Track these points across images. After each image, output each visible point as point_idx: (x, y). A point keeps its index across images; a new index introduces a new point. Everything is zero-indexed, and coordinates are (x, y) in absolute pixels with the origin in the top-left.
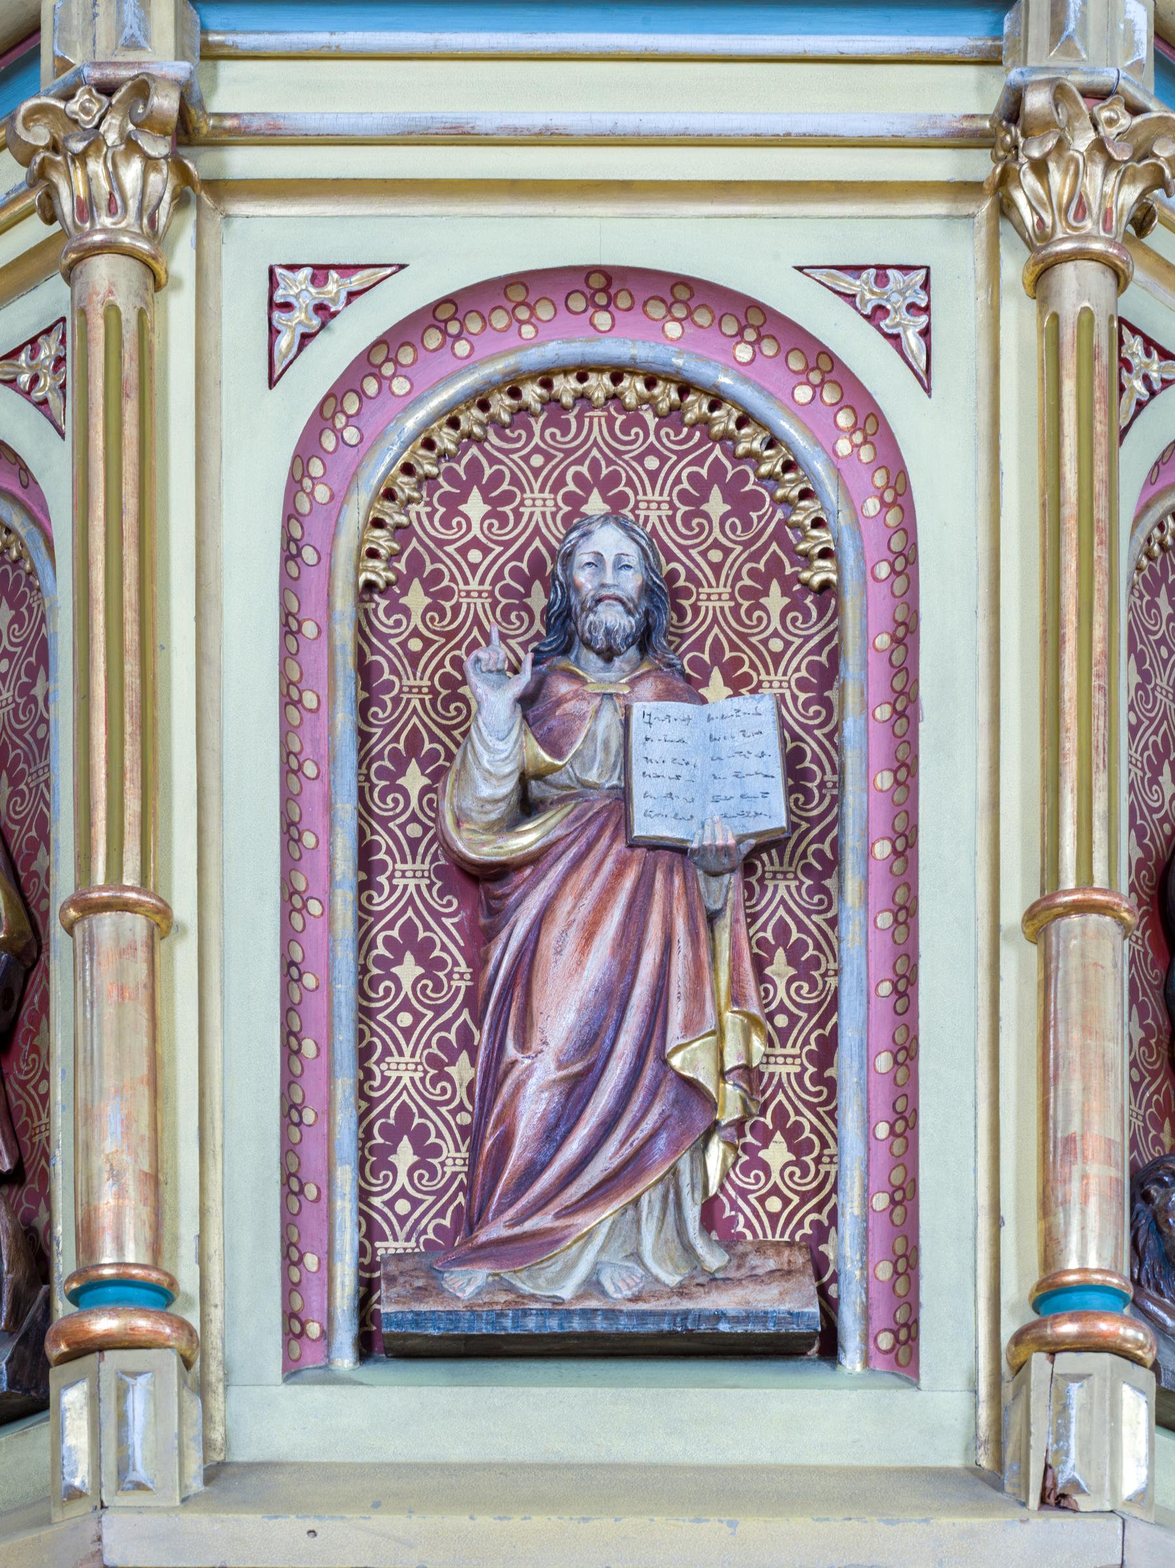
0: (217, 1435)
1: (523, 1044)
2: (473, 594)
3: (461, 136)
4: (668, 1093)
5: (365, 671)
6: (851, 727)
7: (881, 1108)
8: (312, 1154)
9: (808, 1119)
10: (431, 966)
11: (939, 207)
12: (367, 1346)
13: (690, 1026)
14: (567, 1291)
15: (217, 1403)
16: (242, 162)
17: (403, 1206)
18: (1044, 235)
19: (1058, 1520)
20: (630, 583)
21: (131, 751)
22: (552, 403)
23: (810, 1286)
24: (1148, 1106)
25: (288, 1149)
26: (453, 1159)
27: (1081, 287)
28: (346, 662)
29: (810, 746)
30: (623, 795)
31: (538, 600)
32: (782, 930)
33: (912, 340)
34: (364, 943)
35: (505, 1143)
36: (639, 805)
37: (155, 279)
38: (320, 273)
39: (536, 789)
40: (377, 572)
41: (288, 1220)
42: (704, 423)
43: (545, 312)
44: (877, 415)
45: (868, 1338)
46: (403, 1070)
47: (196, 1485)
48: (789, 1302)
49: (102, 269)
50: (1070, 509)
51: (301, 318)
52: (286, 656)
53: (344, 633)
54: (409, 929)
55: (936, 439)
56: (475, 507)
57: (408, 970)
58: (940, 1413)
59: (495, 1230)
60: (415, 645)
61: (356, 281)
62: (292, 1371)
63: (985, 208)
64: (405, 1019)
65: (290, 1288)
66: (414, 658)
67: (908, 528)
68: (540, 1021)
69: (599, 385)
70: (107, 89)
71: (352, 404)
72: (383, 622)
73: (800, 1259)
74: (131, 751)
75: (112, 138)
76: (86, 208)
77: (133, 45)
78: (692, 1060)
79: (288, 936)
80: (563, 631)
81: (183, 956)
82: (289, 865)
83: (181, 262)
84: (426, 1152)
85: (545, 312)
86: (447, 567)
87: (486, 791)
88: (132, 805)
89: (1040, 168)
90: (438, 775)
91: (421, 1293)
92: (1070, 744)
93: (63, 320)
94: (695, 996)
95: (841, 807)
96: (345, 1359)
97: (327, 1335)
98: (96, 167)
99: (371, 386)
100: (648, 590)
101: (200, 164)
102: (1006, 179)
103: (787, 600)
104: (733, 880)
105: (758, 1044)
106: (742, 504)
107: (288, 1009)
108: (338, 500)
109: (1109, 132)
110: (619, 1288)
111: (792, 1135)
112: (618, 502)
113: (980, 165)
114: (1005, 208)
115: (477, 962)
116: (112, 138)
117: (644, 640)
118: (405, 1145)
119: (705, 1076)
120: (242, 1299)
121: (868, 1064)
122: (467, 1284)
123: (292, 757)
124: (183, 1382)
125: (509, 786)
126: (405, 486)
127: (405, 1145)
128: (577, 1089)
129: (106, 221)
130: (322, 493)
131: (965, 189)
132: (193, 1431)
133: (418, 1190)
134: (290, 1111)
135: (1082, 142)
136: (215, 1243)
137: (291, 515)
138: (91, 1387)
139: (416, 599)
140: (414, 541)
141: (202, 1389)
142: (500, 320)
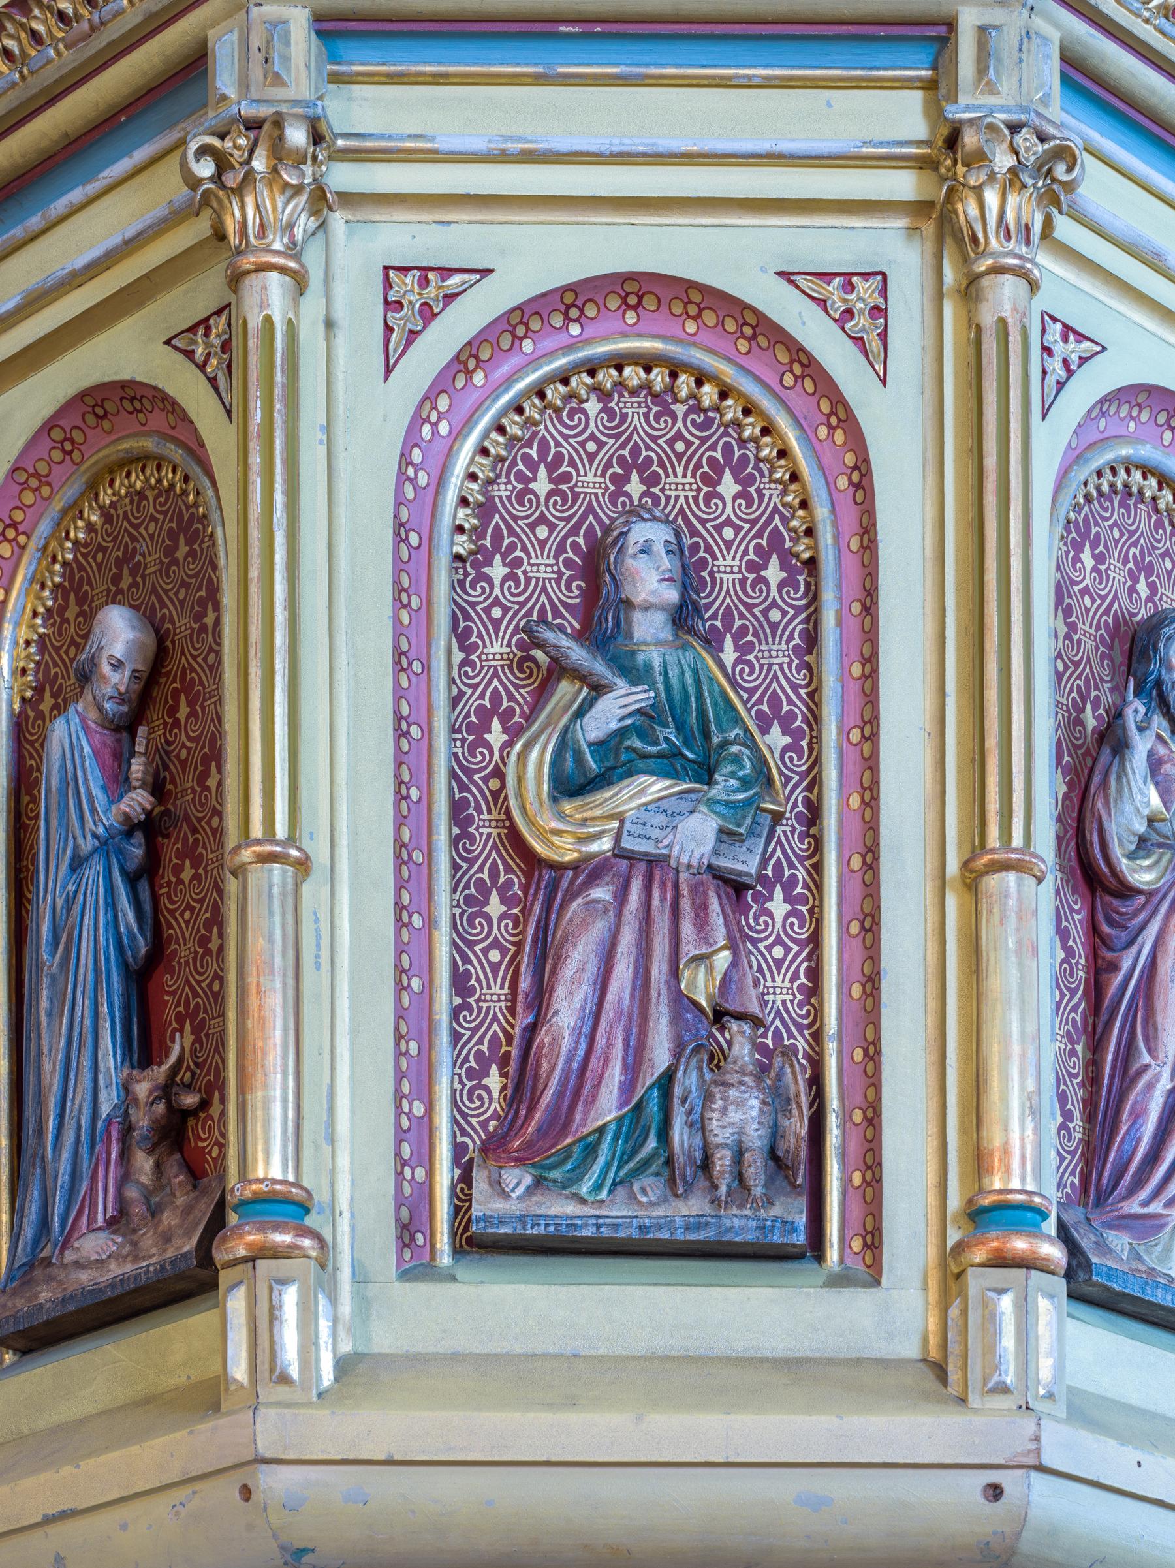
24: (1098, 628)
38: (878, 311)
58: (896, 1315)
60: (497, 613)
66: (497, 623)
93: (229, 305)
95: (821, 766)
103: (784, 575)
123: (403, 786)
138: (248, 1289)
140: (497, 516)
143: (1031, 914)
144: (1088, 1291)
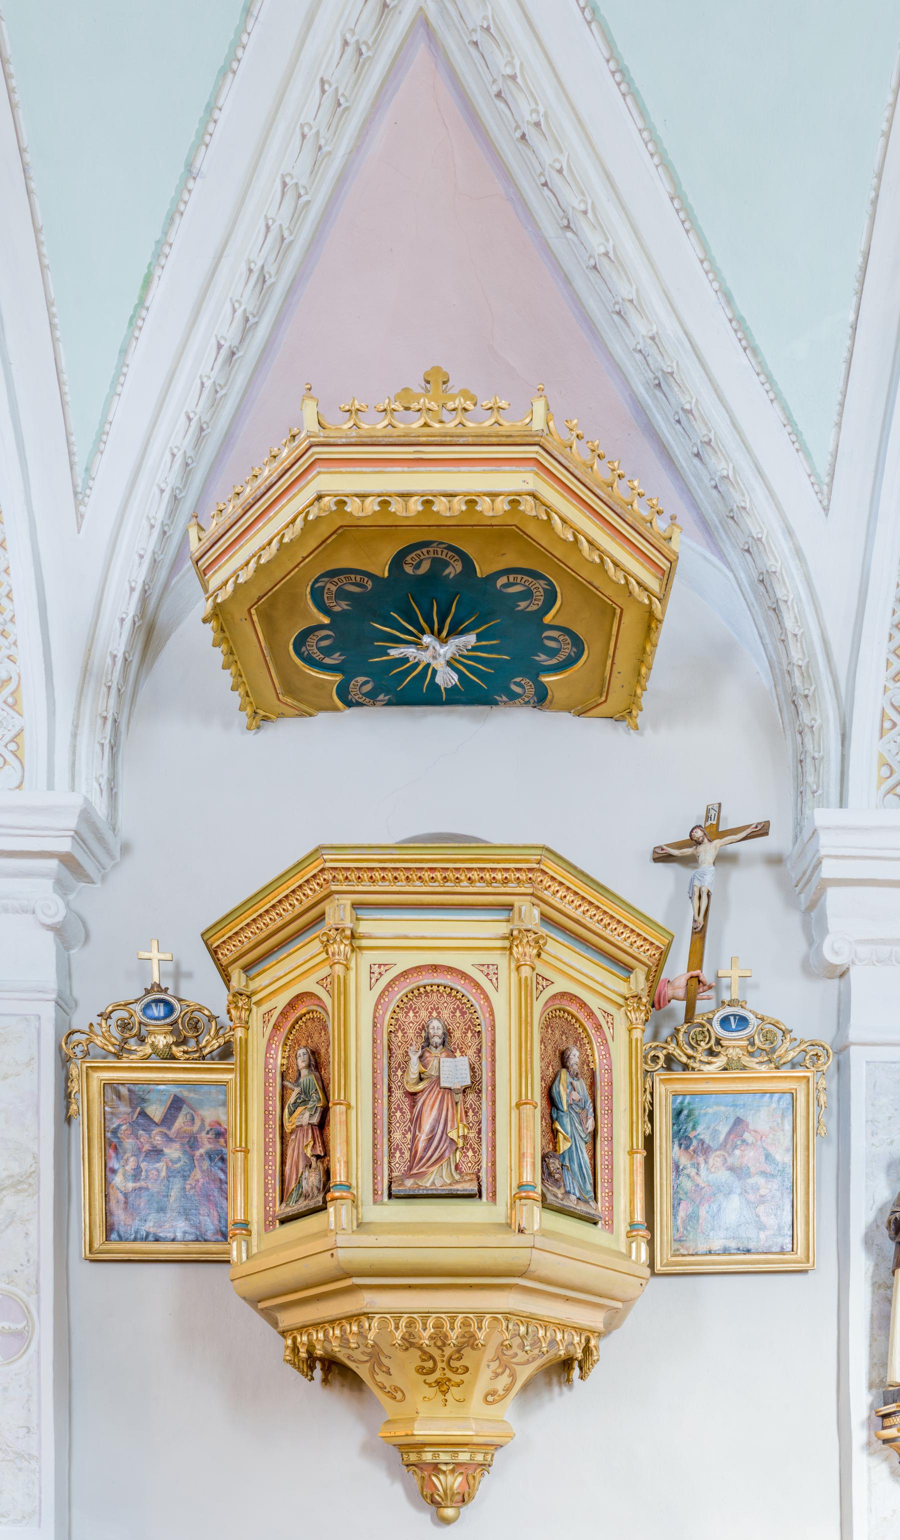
0: (360, 1216)
1: (419, 1131)
2: (411, 1033)
3: (406, 937)
4: (448, 1141)
5: (390, 1049)
6: (484, 1063)
7: (490, 1145)
8: (379, 1154)
9: (476, 1146)
10: (403, 1113)
11: (499, 952)
12: (390, 1196)
13: (452, 1127)
14: (428, 1185)
15: (360, 1209)
16: (364, 943)
17: (397, 1165)
18: (518, 960)
19: (521, 1236)
20: (440, 1032)
21: (342, 1070)
22: (426, 992)
23: (476, 1183)
25: (374, 1154)
26: (407, 1155)
27: (526, 971)
28: (386, 1049)
29: (476, 1066)
30: (439, 1077)
31: (423, 1034)
32: (471, 1105)
33: (494, 980)
34: (389, 1108)
35: (416, 1152)
36: (442, 1080)
37: (347, 968)
38: (380, 966)
39: (422, 1076)
40: (392, 1028)
41: (374, 1169)
42: (456, 996)
43: (424, 973)
44: (487, 996)
45: (487, 1194)
46: (397, 1136)
47: (355, 1228)
48: (472, 1187)
49: (337, 967)
50: (523, 1019)
51: (376, 975)
52: (374, 1048)
53: (385, 1042)
54: (398, 1105)
55: (499, 1001)
56: (411, 1014)
57: (398, 1114)
59: (414, 1171)
61: (387, 968)
62: (375, 1202)
63: (508, 953)
64: (398, 1125)
65: (374, 1184)
66: (399, 1047)
67: (494, 1020)
68: (423, 1127)
69: (435, 988)
70: (337, 930)
71: (387, 993)
72: (393, 1039)
73: (474, 1177)
74: (342, 1070)
75: (338, 939)
76: (333, 954)
77: (342, 920)
78: (453, 1135)
79: (374, 1108)
80: (427, 1042)
81: (353, 1113)
82: (374, 1092)
83: (353, 964)
84: (402, 1154)
85: (424, 973)
86: (406, 1027)
87: (412, 1076)
88: (342, 1082)
89: (517, 946)
90: (404, 1072)
91: (400, 1185)
92: (523, 1069)
94: (453, 1121)
96: (386, 1199)
97: (382, 1194)
98: (335, 946)
99: (390, 989)
100: (444, 1034)
101: (357, 943)
102: (511, 948)
104: (461, 1095)
105: (466, 1131)
106: (463, 1014)
107: (374, 1124)
108: (385, 1013)
109: (530, 939)
110: (438, 1184)
111: (473, 1149)
112: (439, 1013)
113: (506, 943)
114: (511, 953)
115: (411, 1113)
116: (338, 939)
117: (443, 1043)
118: (398, 1152)
119: (455, 1138)
120: (365, 1190)
121: (487, 1135)
122: (409, 1183)
124: (352, 1206)
125: (417, 1076)
126: (397, 1010)
127: (398, 1152)
128: (430, 1140)
129: (337, 957)
130: (381, 1012)
131: (504, 948)
132: (354, 1217)
133: (401, 1162)
134: (375, 1146)
135: (525, 941)
136: (360, 1175)
137: (375, 1017)
139: (400, 1034)
141: (357, 1207)
142: (415, 975)
143: (535, 1118)
144: (546, 1205)
